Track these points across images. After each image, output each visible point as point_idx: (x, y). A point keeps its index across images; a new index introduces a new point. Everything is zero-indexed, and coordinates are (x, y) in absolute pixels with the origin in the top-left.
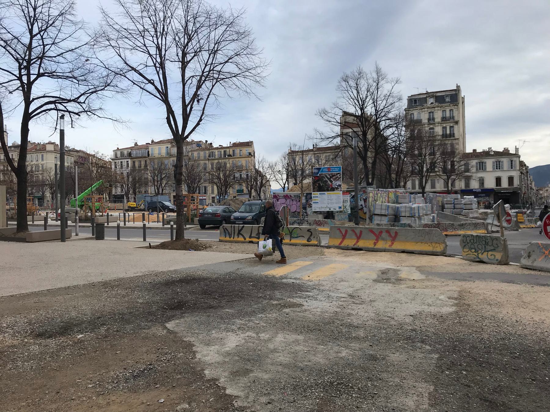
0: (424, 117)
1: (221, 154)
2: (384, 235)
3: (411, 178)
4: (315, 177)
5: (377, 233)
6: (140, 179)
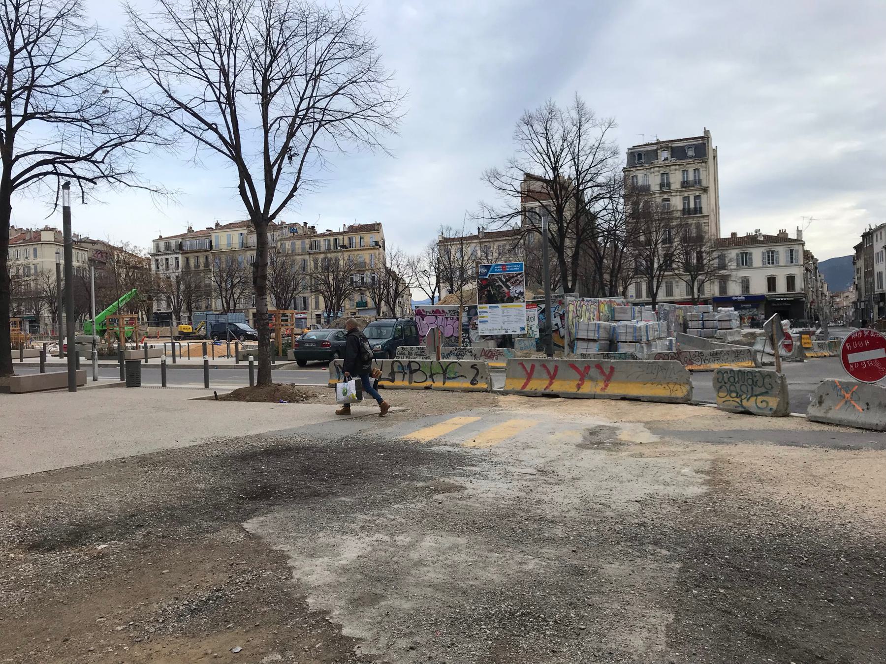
0: (654, 181)
1: (329, 245)
2: (593, 372)
3: (634, 281)
4: (482, 280)
5: (582, 369)
6: (198, 287)
